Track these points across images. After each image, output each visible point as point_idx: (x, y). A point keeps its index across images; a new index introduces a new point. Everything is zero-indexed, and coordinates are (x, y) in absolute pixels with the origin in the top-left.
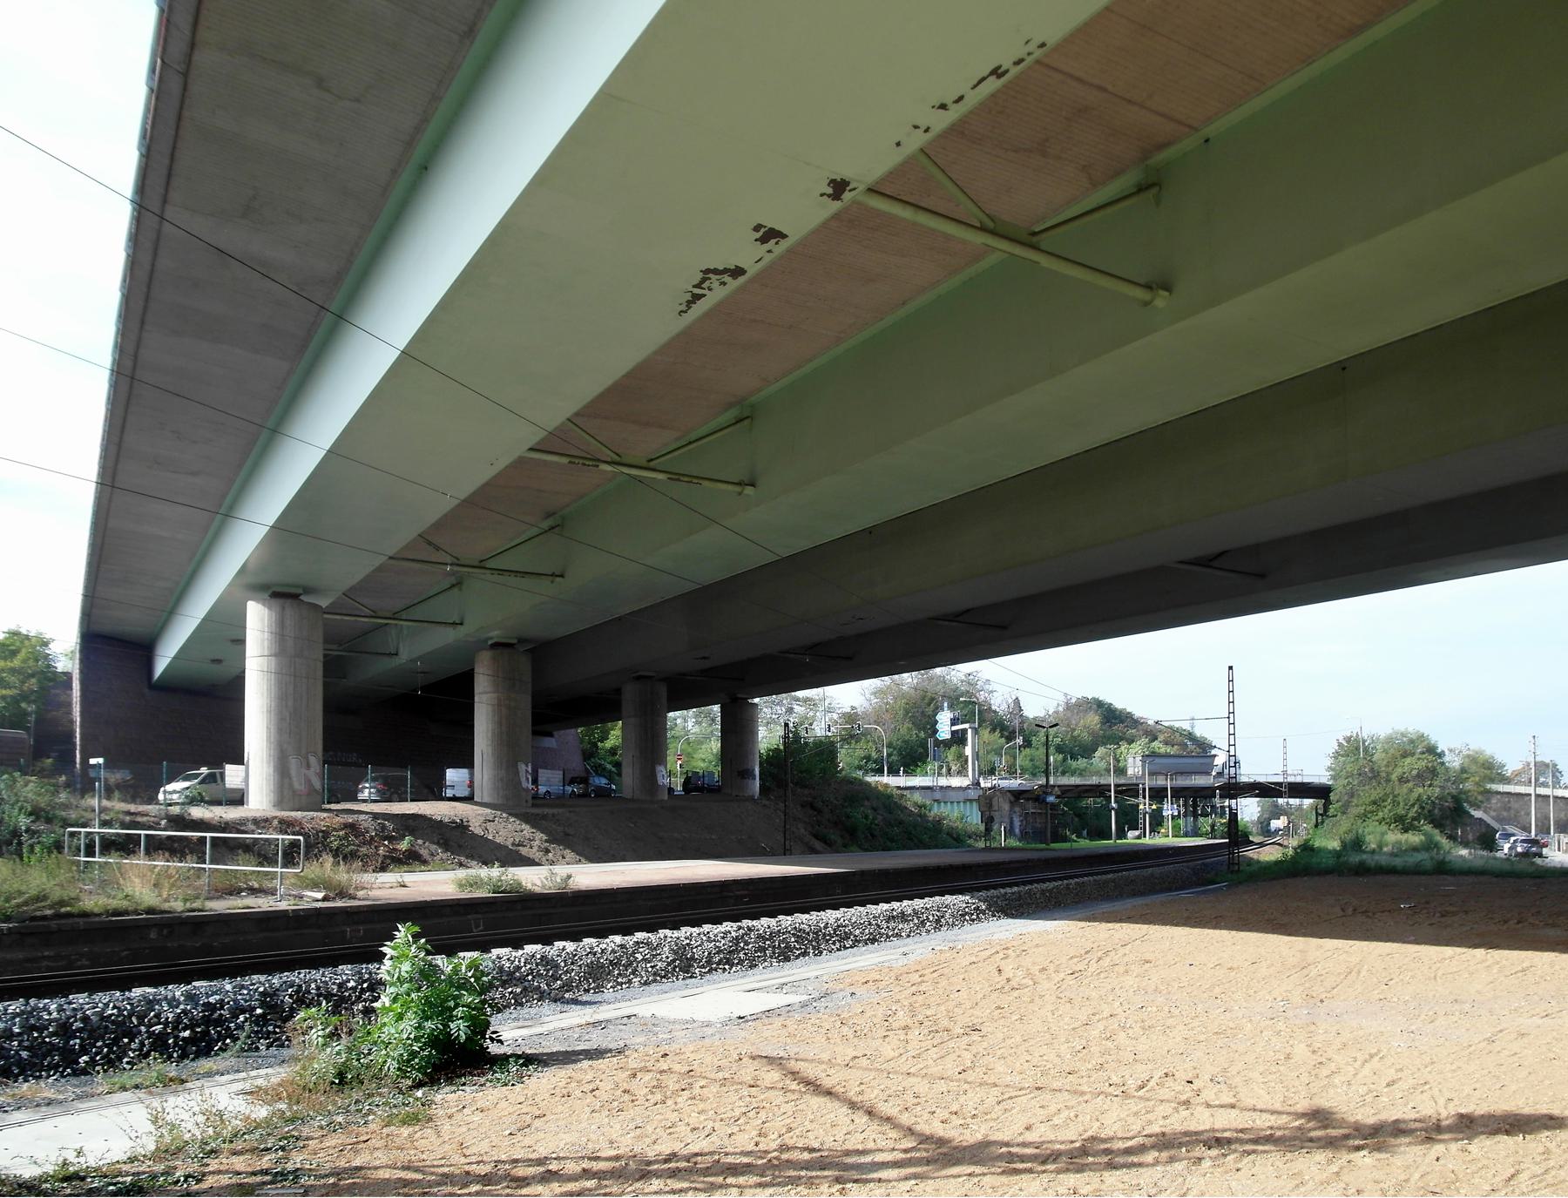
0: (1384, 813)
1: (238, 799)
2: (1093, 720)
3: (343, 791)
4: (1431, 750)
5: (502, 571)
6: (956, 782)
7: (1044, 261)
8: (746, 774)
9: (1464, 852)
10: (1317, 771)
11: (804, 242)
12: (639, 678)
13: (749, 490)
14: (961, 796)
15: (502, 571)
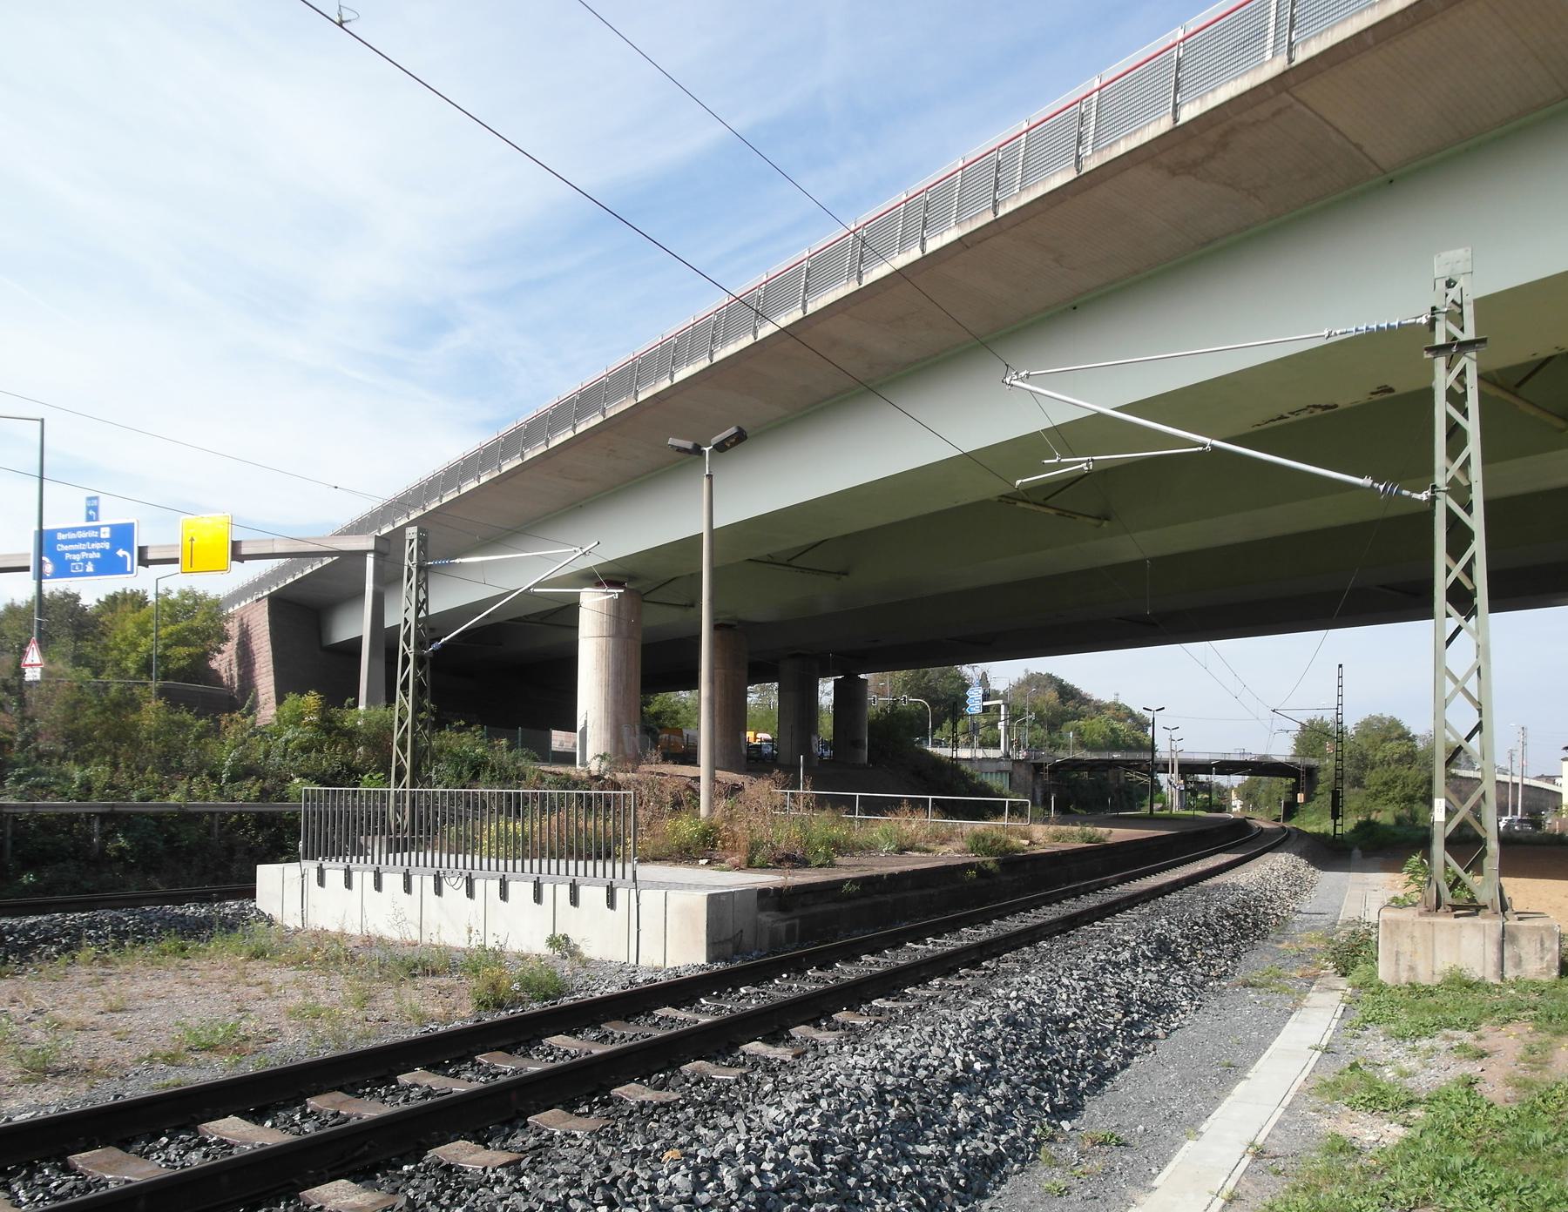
0: (1396, 792)
1: (568, 758)
2: (1051, 696)
3: (638, 760)
4: (1405, 736)
5: (803, 569)
6: (992, 753)
7: (1521, 405)
8: (857, 744)
9: (1040, 831)
10: (1282, 749)
11: (1398, 397)
12: (793, 656)
13: (1105, 524)
14: (994, 767)
15: (803, 569)
